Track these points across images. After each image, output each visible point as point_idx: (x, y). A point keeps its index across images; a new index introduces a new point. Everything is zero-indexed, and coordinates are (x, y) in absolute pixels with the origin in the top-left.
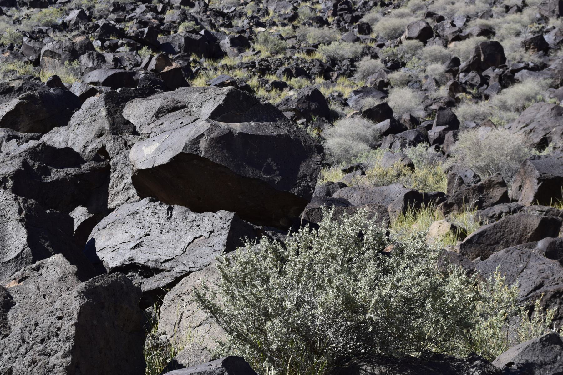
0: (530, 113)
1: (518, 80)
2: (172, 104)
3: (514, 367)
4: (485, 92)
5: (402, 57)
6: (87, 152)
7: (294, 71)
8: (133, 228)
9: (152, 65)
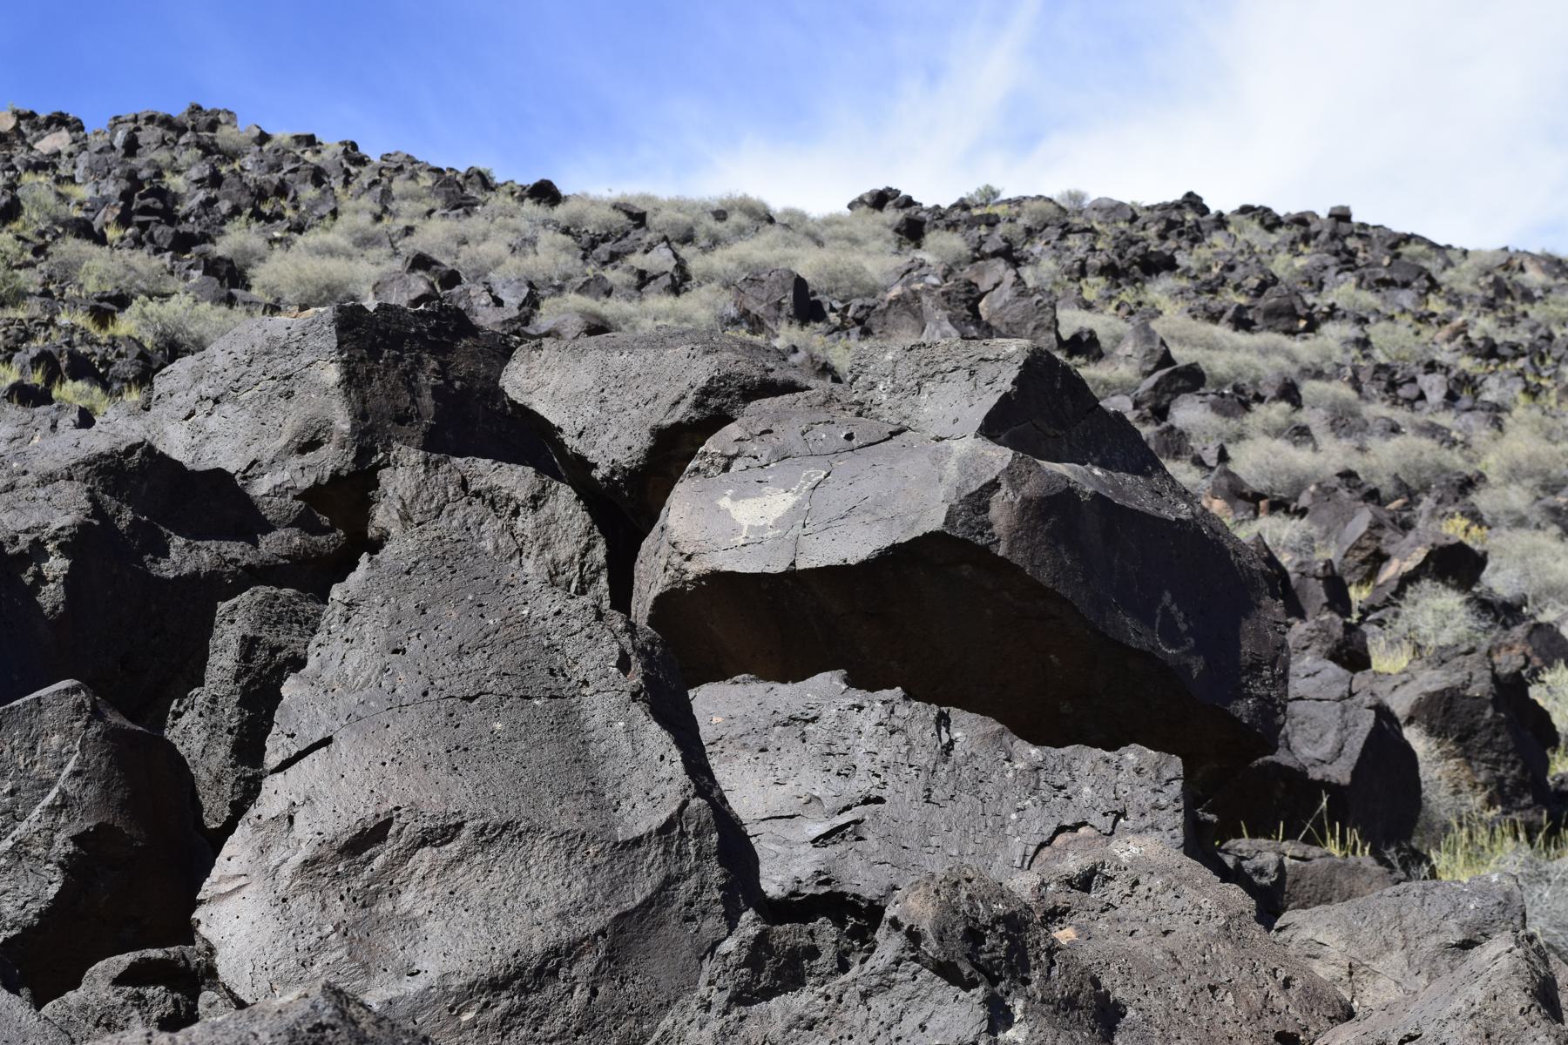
7: (64, 363)
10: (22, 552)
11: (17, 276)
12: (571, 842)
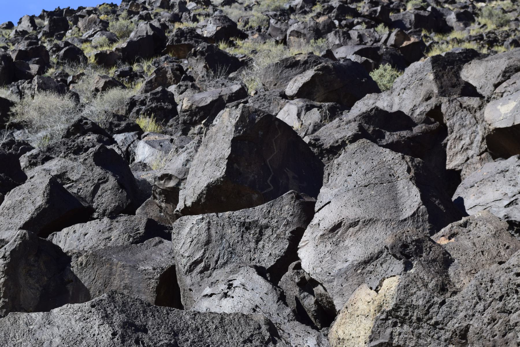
6: (415, 115)
8: (504, 186)
9: (392, 40)
10: (339, 145)
11: (505, 16)
12: (387, 222)
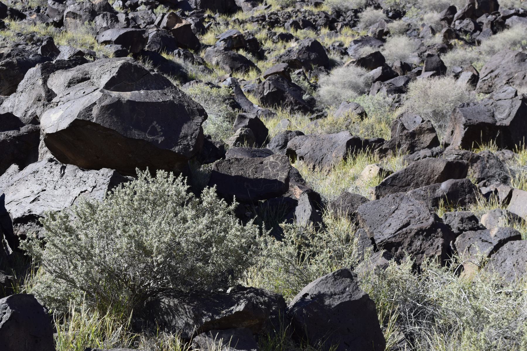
0: (496, 60)
1: (508, 26)
2: (81, 76)
3: (308, 297)
4: (478, 38)
5: (404, 7)
6: (28, 116)
7: (301, 23)
8: (33, 185)
9: (164, 23)
